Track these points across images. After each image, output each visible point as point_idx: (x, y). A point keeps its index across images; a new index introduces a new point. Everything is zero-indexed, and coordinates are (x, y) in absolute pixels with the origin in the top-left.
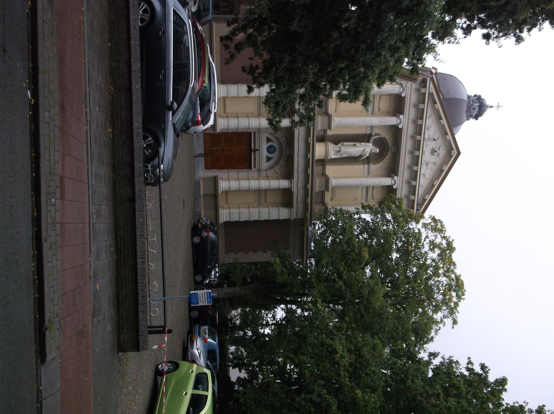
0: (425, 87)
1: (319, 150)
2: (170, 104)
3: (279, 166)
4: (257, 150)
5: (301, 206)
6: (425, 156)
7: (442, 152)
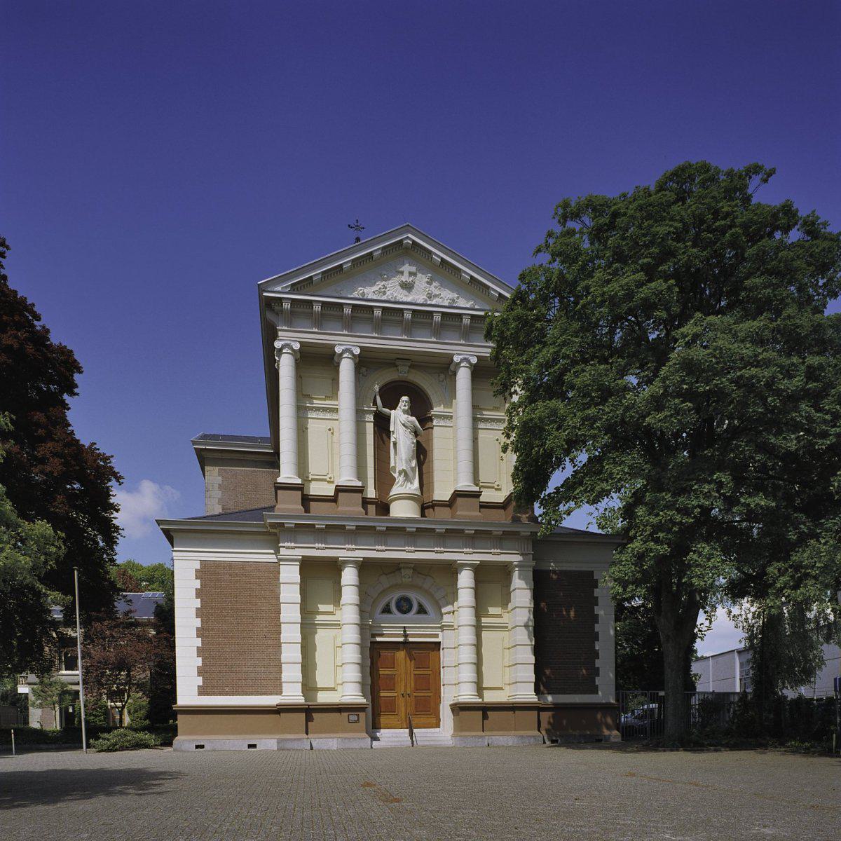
1: (402, 510)
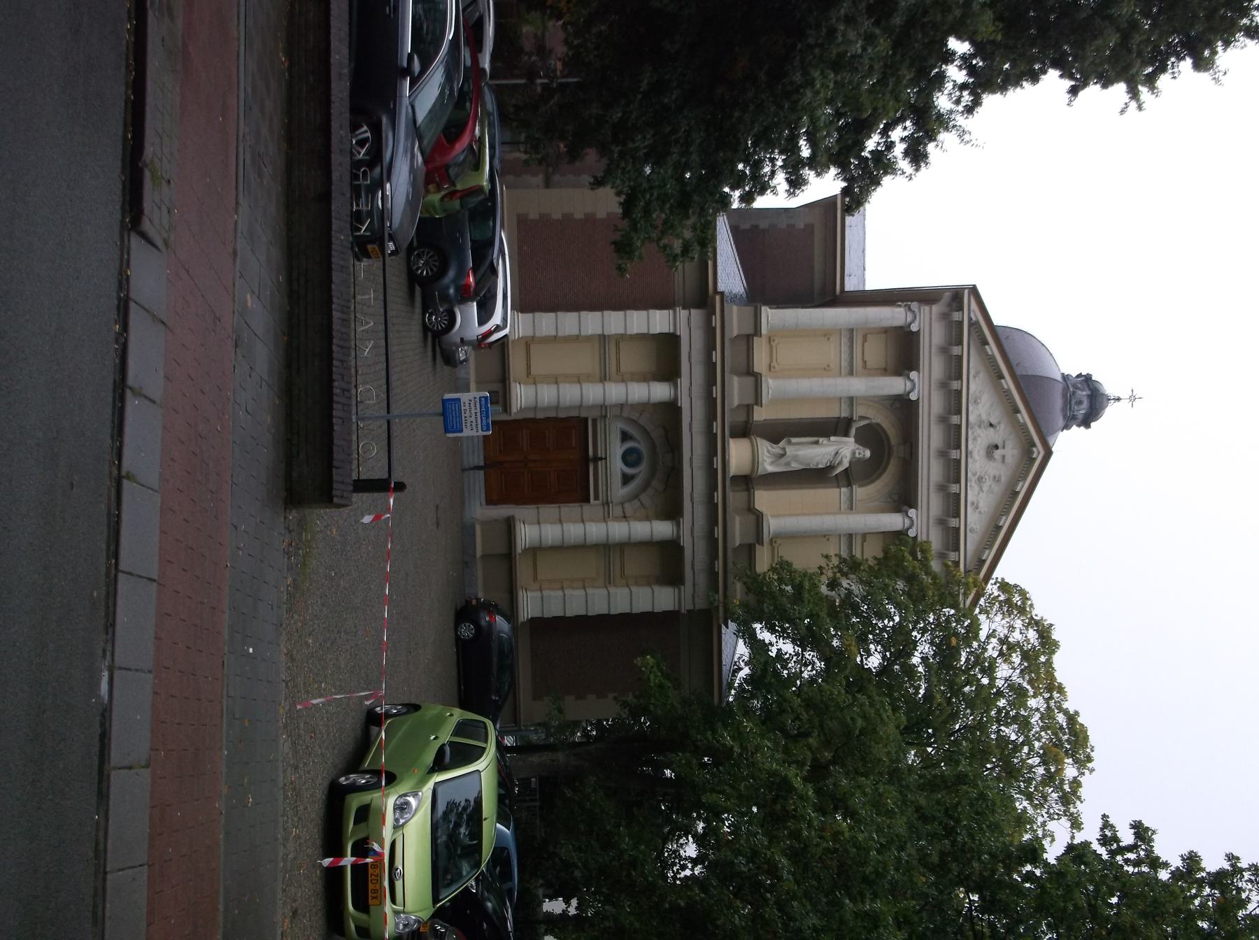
0: (961, 309)
1: (738, 454)
2: (405, 65)
3: (650, 491)
4: (601, 459)
5: (702, 580)
6: (975, 461)
7: (1011, 452)
